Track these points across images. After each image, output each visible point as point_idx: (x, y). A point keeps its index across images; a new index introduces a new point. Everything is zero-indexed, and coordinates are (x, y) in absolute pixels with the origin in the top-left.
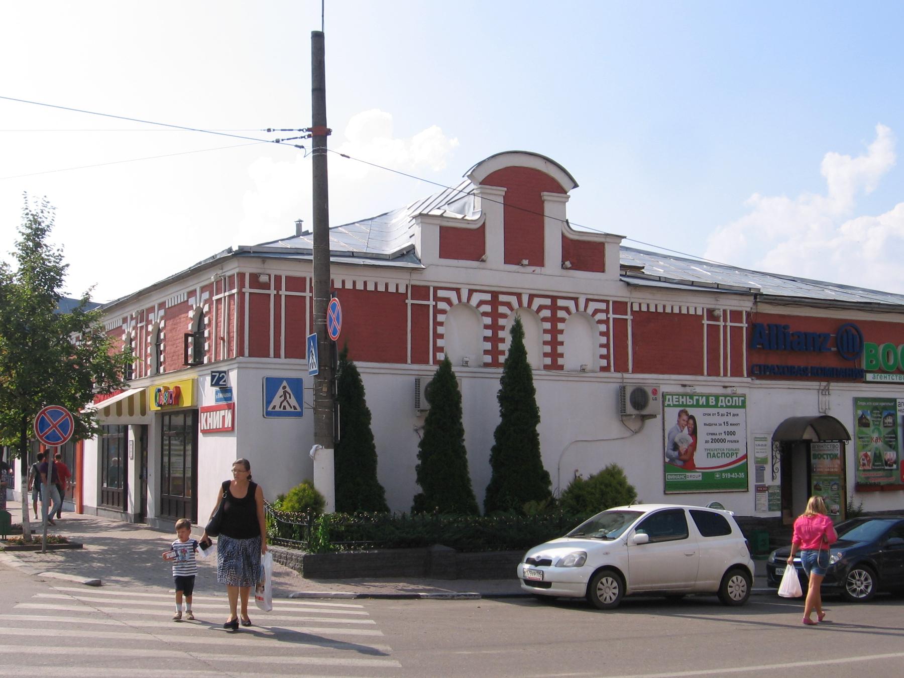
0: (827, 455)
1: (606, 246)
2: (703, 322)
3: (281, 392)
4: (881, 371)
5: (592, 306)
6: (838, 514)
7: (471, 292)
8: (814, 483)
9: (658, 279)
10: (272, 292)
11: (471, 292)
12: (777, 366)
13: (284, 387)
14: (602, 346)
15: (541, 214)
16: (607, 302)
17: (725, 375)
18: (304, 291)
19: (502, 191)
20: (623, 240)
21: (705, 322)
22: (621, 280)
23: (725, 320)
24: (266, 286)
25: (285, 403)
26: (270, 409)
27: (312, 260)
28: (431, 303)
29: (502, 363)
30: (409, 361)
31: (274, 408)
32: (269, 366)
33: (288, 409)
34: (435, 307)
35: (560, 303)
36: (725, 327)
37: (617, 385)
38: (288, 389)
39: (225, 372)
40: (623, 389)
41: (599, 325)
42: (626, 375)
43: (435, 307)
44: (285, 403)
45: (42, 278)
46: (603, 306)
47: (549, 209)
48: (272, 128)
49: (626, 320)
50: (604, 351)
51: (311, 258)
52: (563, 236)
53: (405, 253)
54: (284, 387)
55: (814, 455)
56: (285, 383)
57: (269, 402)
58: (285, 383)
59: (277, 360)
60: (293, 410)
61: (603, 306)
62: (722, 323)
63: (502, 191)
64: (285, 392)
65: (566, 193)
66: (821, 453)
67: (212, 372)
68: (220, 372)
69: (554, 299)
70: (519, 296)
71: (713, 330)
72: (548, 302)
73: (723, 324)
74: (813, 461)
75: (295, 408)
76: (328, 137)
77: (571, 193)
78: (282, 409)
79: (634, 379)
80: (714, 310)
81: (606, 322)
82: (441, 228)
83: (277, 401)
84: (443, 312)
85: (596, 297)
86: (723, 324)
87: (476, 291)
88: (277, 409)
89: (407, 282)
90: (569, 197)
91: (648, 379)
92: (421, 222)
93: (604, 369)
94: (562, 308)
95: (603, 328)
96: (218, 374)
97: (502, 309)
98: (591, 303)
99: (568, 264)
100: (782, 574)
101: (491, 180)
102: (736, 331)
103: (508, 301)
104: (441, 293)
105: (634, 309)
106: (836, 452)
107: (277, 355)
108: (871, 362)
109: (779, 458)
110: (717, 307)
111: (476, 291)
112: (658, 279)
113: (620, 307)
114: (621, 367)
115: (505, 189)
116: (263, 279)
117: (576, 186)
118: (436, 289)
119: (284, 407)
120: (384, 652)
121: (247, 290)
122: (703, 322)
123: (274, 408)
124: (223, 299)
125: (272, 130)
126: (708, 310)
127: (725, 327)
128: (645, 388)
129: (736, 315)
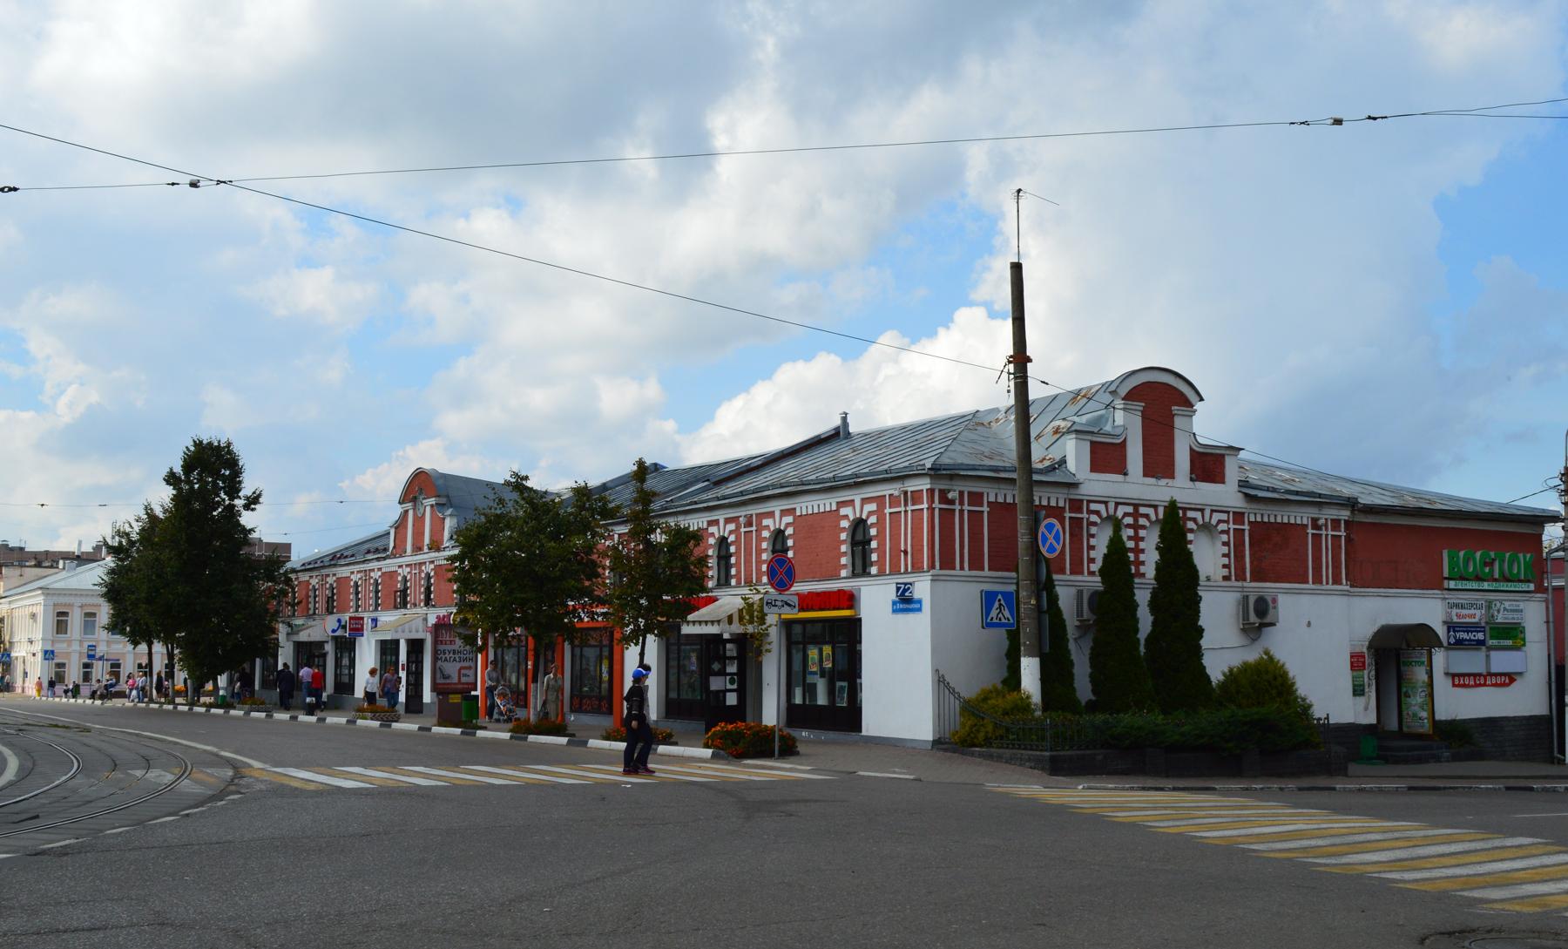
0: (1415, 662)
1: (1227, 459)
2: (1308, 531)
3: (997, 605)
4: (1462, 578)
5: (1216, 517)
6: (1426, 721)
7: (1117, 504)
8: (1404, 690)
10: (957, 507)
11: (1117, 504)
13: (999, 600)
14: (1224, 555)
15: (1172, 427)
16: (1228, 512)
17: (962, 568)
18: (1082, 513)
19: (1140, 405)
20: (1241, 452)
21: (1310, 531)
22: (1239, 491)
23: (962, 503)
24: (952, 502)
25: (1000, 615)
27: (1015, 479)
28: (1085, 515)
29: (1139, 570)
30: (1068, 572)
32: (1304, 592)
33: (1003, 620)
34: (1088, 519)
35: (1143, 510)
36: (1327, 535)
37: (1238, 595)
38: (1002, 602)
39: (911, 584)
40: (1246, 598)
41: (1222, 535)
42: (1245, 584)
43: (1088, 519)
44: (1000, 615)
46: (1224, 517)
47: (1179, 422)
49: (1244, 530)
50: (1226, 561)
51: (1014, 476)
52: (1191, 449)
53: (1057, 466)
54: (999, 600)
55: (1403, 662)
56: (1000, 597)
57: (988, 615)
58: (1000, 597)
59: (962, 573)
60: (1006, 621)
61: (1224, 517)
62: (1324, 532)
63: (1140, 405)
64: (1000, 605)
65: (1192, 406)
66: (1410, 660)
67: (897, 584)
68: (905, 584)
69: (1136, 506)
70: (1155, 507)
71: (1317, 537)
72: (1130, 509)
73: (959, 507)
74: (1403, 668)
75: (1009, 620)
76: (1028, 364)
77: (1198, 406)
78: (998, 621)
79: (1255, 588)
80: (1317, 519)
81: (1227, 532)
82: (1093, 443)
83: (994, 613)
84: (1143, 527)
85: (1193, 506)
86: (959, 507)
87: (1216, 511)
88: (995, 620)
89: (1066, 496)
90: (1195, 411)
91: (1268, 588)
92: (1076, 438)
93: (1226, 578)
94: (1190, 519)
95: (1224, 538)
96: (903, 586)
97: (1142, 521)
98: (1215, 514)
99: (1193, 476)
101: (1131, 396)
102: (975, 517)
103: (1194, 516)
104: (1093, 507)
105: (1251, 520)
106: (1423, 659)
107: (962, 568)
108: (1454, 568)
110: (1321, 516)
111: (1216, 511)
113: (1239, 517)
114: (1240, 577)
115: (1143, 404)
116: (950, 496)
117: (1202, 399)
118: (1089, 502)
119: (1000, 619)
121: (936, 505)
122: (1308, 531)
124: (903, 513)
126: (1312, 519)
127: (962, 511)
128: (1266, 597)
129: (1336, 523)
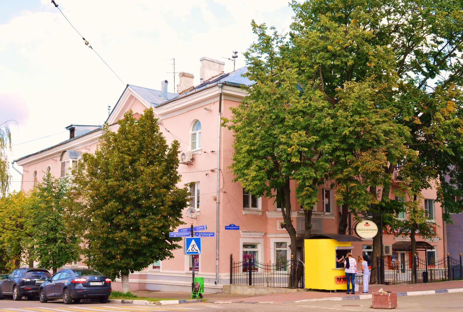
9: (210, 280)
12: (421, 191)
25: (193, 249)
26: (188, 251)
31: (189, 251)
33: (195, 251)
44: (193, 249)
45: (421, 134)
48: (84, 42)
60: (196, 251)
75: (197, 250)
78: (192, 251)
88: (190, 251)
100: (371, 285)
109: (385, 263)
112: (210, 280)
119: (193, 250)
120: (327, 236)
123: (189, 251)
125: (89, 45)
